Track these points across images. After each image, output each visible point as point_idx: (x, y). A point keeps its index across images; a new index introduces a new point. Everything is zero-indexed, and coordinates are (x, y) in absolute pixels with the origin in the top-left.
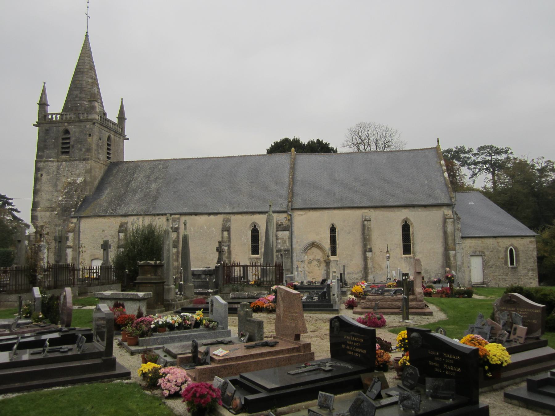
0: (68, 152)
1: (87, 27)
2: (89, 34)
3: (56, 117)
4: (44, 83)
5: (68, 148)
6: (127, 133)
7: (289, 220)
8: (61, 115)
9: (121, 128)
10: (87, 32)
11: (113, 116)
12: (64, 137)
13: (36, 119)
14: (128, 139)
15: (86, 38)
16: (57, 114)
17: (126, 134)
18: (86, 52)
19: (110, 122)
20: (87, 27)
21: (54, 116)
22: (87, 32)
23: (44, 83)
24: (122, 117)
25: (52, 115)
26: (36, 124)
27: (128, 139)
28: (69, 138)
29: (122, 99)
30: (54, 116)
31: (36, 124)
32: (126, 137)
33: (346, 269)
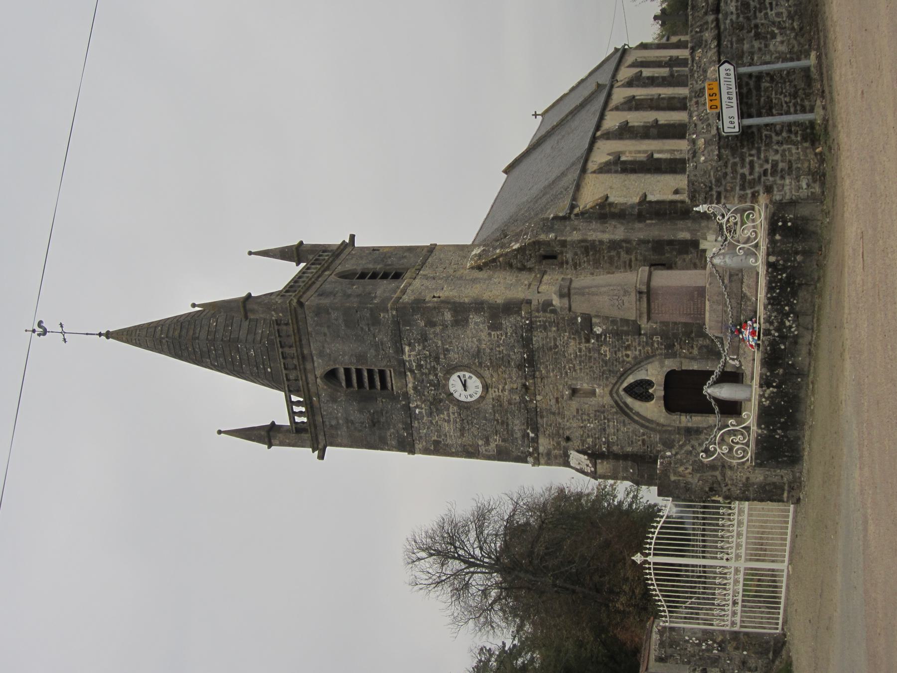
0: (382, 373)
1: (87, 334)
2: (104, 332)
3: (298, 403)
4: (220, 432)
5: (359, 372)
6: (335, 239)
7: (529, 313)
8: (289, 392)
9: (324, 251)
10: (100, 334)
11: (290, 270)
12: (344, 384)
13: (307, 453)
14: (352, 237)
15: (113, 338)
16: (290, 403)
17: (339, 242)
18: (132, 336)
19: (304, 273)
20: (87, 334)
21: (296, 409)
22: (100, 334)
23: (220, 432)
24: (294, 253)
25: (292, 414)
26: (317, 452)
27: (352, 237)
28: (347, 371)
29: (250, 253)
30: (296, 409)
31: (317, 452)
32: (347, 241)
33: (611, 60)
